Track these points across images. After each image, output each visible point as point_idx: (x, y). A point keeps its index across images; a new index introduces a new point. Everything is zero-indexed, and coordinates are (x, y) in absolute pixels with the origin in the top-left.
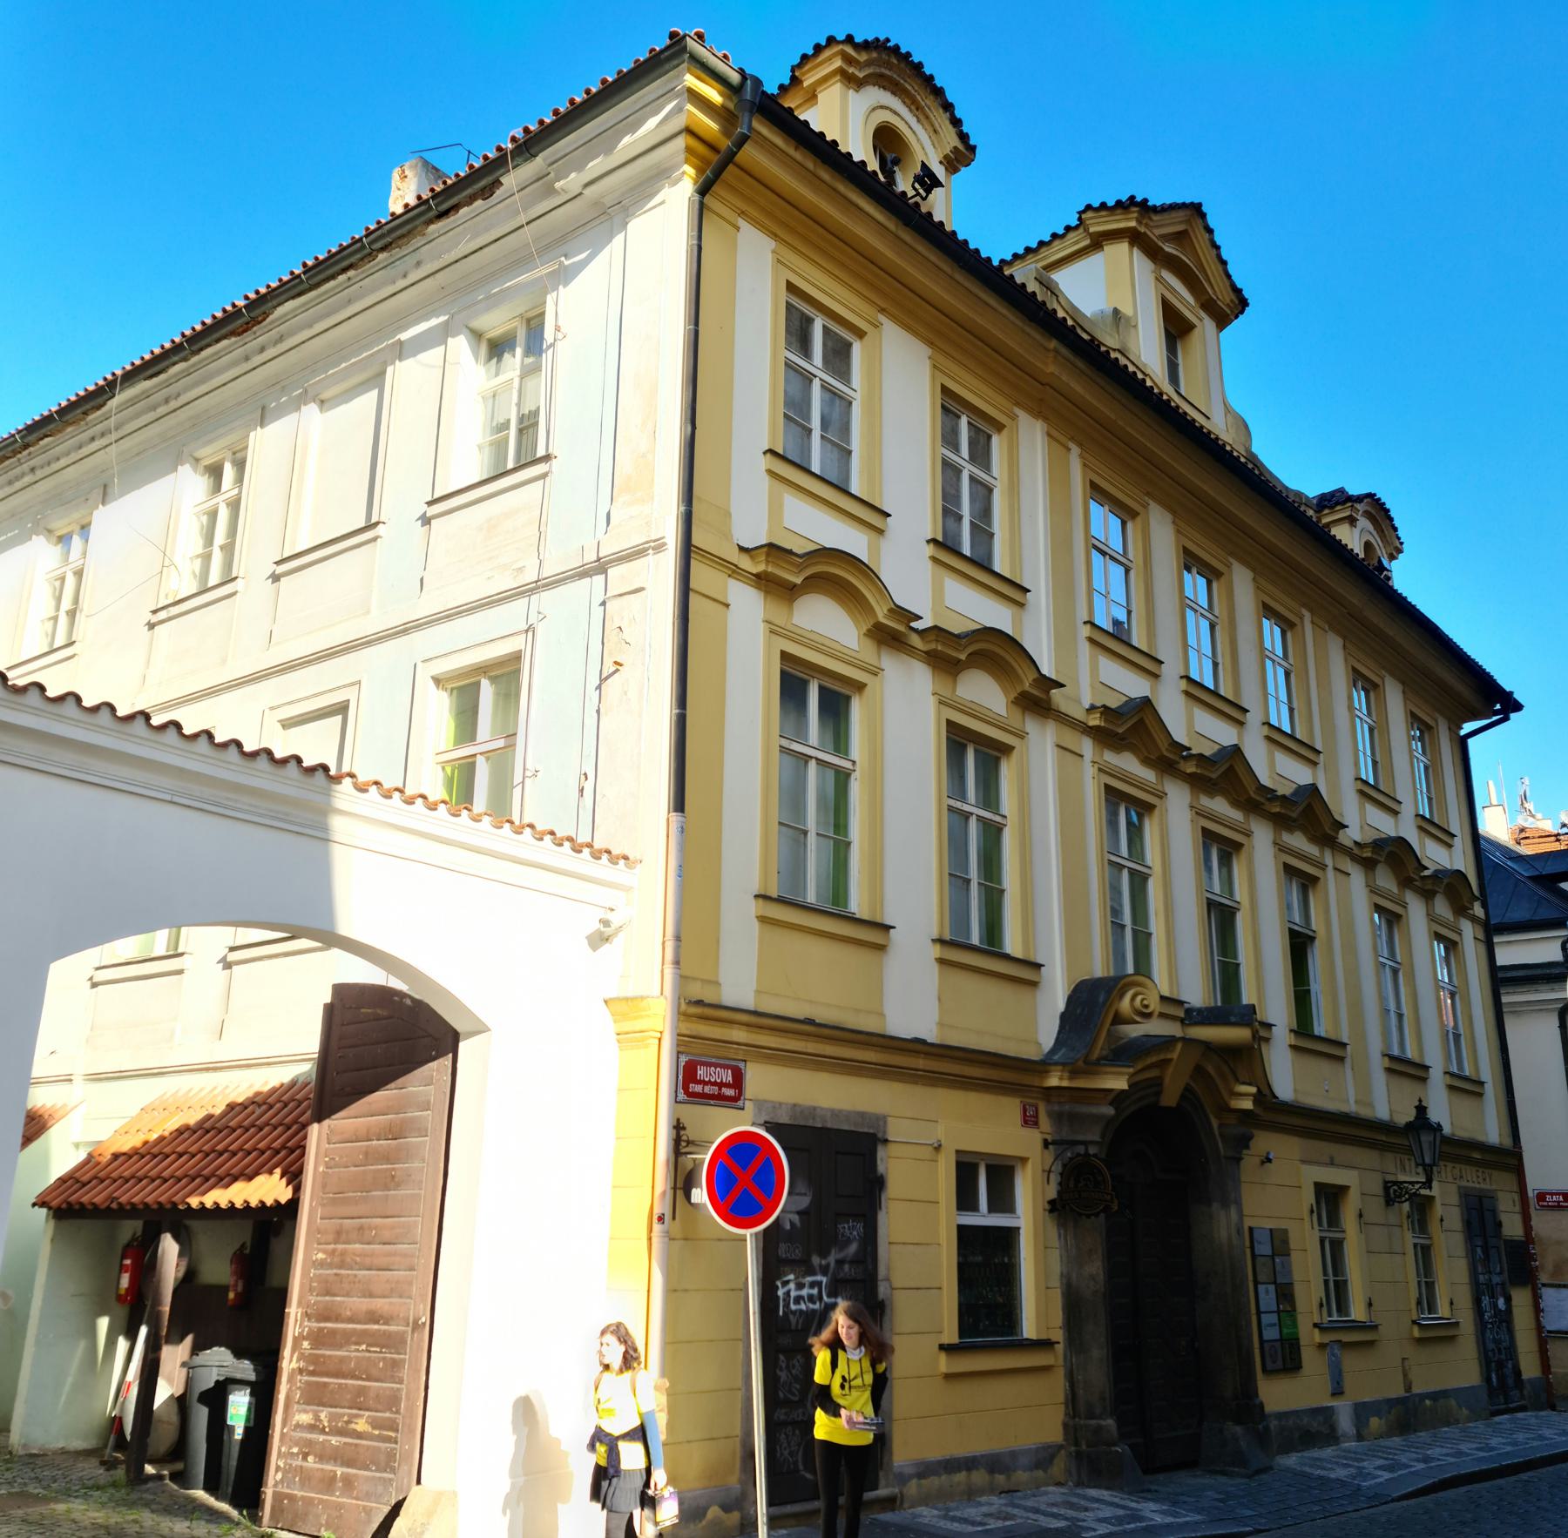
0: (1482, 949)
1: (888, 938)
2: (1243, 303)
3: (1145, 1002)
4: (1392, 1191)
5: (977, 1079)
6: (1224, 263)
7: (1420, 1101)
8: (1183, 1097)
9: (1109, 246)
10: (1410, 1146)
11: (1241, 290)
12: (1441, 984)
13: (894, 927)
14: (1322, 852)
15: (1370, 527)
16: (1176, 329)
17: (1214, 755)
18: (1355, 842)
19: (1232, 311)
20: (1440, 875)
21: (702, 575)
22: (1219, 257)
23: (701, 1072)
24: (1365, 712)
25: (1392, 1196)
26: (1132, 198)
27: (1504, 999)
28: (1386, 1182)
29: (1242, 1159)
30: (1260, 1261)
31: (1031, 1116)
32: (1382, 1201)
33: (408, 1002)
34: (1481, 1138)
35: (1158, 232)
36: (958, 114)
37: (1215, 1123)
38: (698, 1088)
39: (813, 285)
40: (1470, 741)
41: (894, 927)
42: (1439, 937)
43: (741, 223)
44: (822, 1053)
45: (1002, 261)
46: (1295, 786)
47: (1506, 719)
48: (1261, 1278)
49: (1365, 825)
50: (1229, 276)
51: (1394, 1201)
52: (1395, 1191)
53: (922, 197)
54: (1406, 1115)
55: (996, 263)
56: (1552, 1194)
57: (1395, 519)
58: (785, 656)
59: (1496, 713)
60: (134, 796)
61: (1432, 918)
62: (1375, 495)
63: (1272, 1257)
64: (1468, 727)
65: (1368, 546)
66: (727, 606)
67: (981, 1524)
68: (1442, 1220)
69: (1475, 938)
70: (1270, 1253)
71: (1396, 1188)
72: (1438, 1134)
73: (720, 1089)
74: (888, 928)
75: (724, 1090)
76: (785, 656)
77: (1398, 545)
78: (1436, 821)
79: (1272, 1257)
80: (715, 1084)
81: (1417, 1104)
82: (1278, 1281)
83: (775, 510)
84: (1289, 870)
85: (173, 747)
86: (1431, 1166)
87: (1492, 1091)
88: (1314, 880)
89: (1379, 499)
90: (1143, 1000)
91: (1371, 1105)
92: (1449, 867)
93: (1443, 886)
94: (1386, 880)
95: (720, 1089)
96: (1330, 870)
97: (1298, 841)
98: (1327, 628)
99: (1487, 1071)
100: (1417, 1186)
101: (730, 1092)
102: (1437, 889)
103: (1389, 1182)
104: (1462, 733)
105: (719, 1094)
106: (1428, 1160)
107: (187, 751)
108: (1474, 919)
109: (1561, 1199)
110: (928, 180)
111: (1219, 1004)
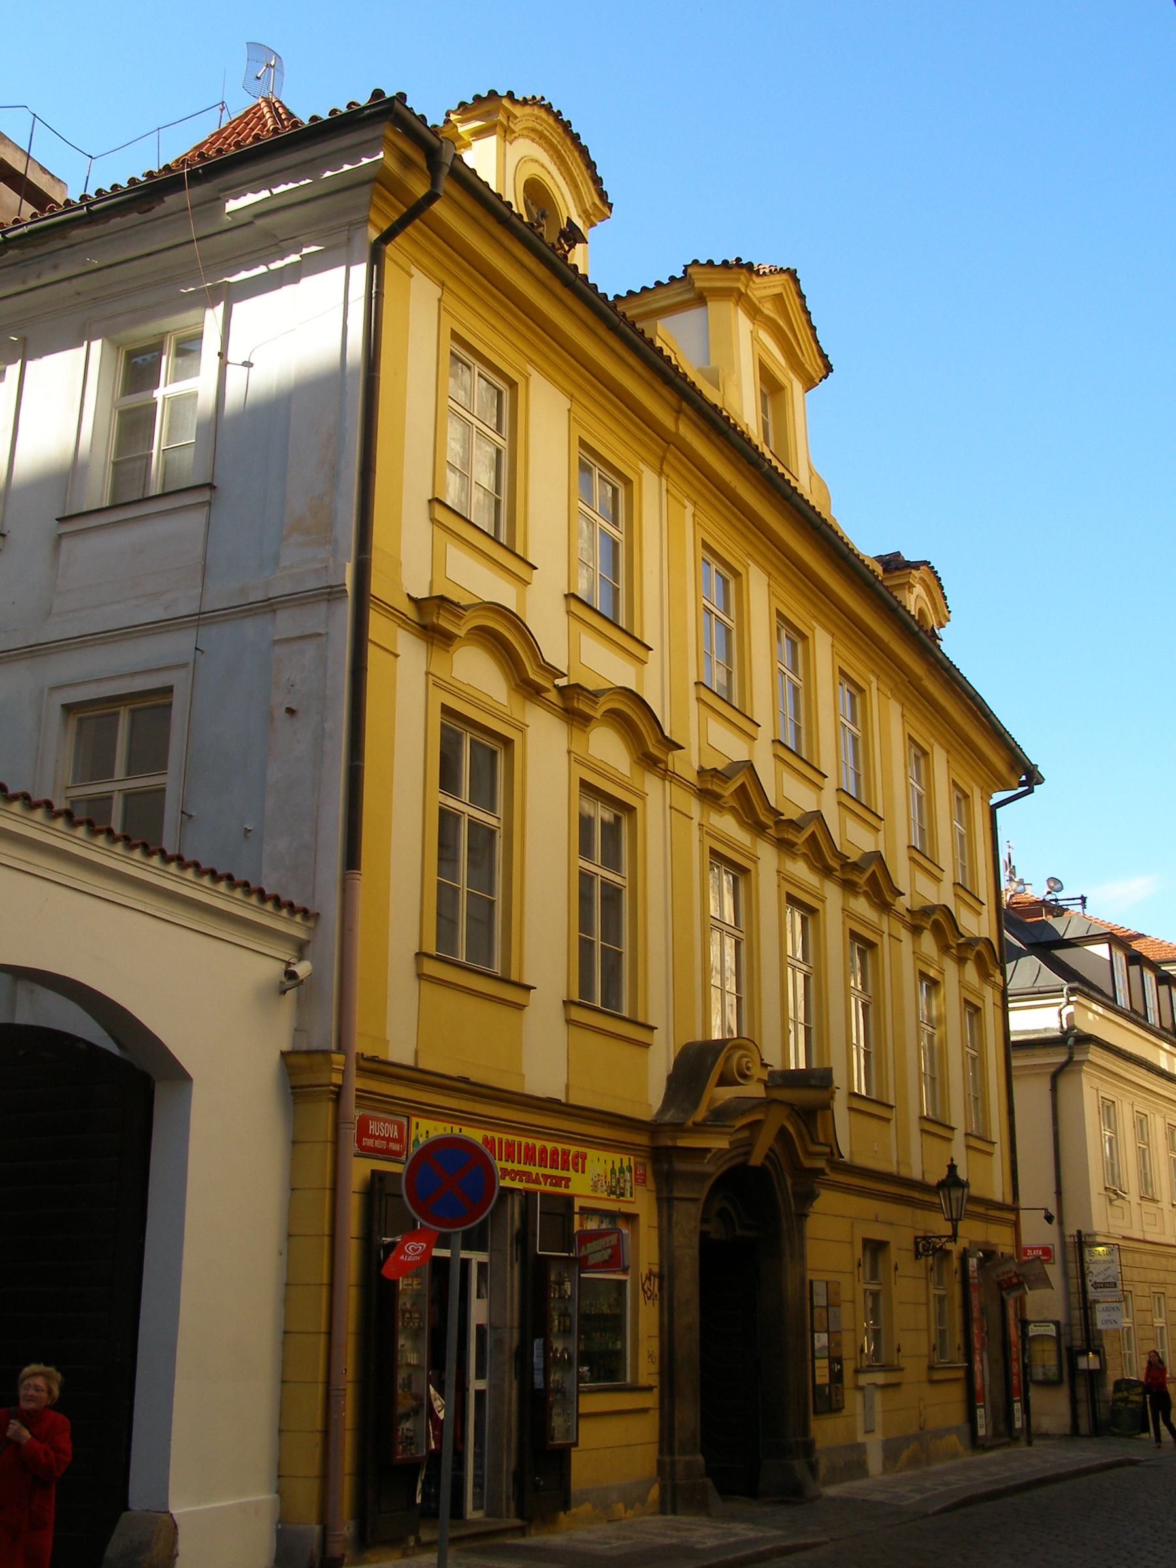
0: (999, 1012)
1: (953, 1134)
2: (829, 368)
3: (750, 1065)
4: (921, 1246)
5: (598, 1138)
6: (813, 329)
7: (952, 1160)
8: (767, 1157)
9: (715, 303)
10: (941, 1204)
11: (827, 356)
12: (789, 960)
13: (657, 1028)
14: (880, 919)
15: (923, 594)
16: (771, 388)
17: (725, 769)
18: (907, 909)
19: (817, 375)
20: (972, 942)
21: (377, 624)
22: (809, 321)
23: (373, 1127)
24: (849, 718)
25: (921, 1250)
26: (738, 260)
27: (1015, 1063)
28: (916, 1238)
29: (806, 1216)
30: (816, 1311)
31: (640, 1175)
32: (912, 1255)
33: (82, 1046)
34: (989, 1196)
35: (759, 293)
36: (599, 173)
37: (789, 1182)
38: (368, 1142)
39: (468, 329)
40: (998, 811)
41: (657, 1028)
42: (792, 900)
43: (414, 270)
44: (561, 1128)
45: (617, 297)
46: (861, 852)
47: (1030, 791)
48: (816, 1327)
49: (706, 746)
50: (817, 342)
51: (922, 1255)
52: (924, 1246)
53: (565, 251)
54: (937, 1175)
55: (611, 298)
56: (1033, 1249)
57: (945, 588)
58: (446, 710)
59: (1022, 784)
60: (155, 919)
61: (962, 984)
62: (929, 563)
63: (827, 1308)
64: (998, 797)
65: (921, 612)
66: (397, 656)
67: (955, 1484)
68: (896, 1269)
69: (994, 1004)
70: (830, 1308)
71: (923, 1242)
72: (966, 1190)
73: (388, 1144)
74: (529, 988)
75: (391, 1144)
76: (446, 710)
77: (947, 613)
78: (472, 520)
79: (827, 1308)
80: (383, 1138)
81: (950, 1163)
82: (830, 1330)
83: (437, 562)
84: (854, 935)
85: (206, 888)
86: (957, 1220)
87: (1000, 1150)
88: (871, 945)
89: (933, 567)
90: (749, 1062)
91: (909, 1165)
92: (977, 936)
93: (930, 923)
94: (928, 943)
95: (388, 1144)
96: (886, 936)
97: (861, 906)
98: (889, 696)
99: (997, 1130)
100: (944, 1240)
101: (395, 1147)
102: (923, 924)
103: (919, 1237)
104: (992, 802)
105: (387, 1148)
106: (954, 1216)
107: (128, 858)
108: (994, 985)
109: (1041, 1253)
110: (573, 236)
111: (802, 1066)
